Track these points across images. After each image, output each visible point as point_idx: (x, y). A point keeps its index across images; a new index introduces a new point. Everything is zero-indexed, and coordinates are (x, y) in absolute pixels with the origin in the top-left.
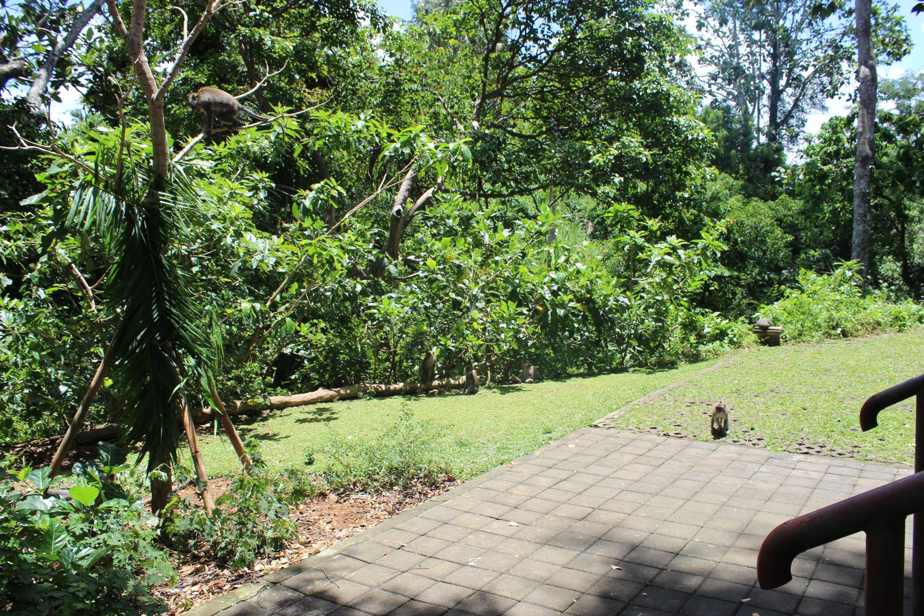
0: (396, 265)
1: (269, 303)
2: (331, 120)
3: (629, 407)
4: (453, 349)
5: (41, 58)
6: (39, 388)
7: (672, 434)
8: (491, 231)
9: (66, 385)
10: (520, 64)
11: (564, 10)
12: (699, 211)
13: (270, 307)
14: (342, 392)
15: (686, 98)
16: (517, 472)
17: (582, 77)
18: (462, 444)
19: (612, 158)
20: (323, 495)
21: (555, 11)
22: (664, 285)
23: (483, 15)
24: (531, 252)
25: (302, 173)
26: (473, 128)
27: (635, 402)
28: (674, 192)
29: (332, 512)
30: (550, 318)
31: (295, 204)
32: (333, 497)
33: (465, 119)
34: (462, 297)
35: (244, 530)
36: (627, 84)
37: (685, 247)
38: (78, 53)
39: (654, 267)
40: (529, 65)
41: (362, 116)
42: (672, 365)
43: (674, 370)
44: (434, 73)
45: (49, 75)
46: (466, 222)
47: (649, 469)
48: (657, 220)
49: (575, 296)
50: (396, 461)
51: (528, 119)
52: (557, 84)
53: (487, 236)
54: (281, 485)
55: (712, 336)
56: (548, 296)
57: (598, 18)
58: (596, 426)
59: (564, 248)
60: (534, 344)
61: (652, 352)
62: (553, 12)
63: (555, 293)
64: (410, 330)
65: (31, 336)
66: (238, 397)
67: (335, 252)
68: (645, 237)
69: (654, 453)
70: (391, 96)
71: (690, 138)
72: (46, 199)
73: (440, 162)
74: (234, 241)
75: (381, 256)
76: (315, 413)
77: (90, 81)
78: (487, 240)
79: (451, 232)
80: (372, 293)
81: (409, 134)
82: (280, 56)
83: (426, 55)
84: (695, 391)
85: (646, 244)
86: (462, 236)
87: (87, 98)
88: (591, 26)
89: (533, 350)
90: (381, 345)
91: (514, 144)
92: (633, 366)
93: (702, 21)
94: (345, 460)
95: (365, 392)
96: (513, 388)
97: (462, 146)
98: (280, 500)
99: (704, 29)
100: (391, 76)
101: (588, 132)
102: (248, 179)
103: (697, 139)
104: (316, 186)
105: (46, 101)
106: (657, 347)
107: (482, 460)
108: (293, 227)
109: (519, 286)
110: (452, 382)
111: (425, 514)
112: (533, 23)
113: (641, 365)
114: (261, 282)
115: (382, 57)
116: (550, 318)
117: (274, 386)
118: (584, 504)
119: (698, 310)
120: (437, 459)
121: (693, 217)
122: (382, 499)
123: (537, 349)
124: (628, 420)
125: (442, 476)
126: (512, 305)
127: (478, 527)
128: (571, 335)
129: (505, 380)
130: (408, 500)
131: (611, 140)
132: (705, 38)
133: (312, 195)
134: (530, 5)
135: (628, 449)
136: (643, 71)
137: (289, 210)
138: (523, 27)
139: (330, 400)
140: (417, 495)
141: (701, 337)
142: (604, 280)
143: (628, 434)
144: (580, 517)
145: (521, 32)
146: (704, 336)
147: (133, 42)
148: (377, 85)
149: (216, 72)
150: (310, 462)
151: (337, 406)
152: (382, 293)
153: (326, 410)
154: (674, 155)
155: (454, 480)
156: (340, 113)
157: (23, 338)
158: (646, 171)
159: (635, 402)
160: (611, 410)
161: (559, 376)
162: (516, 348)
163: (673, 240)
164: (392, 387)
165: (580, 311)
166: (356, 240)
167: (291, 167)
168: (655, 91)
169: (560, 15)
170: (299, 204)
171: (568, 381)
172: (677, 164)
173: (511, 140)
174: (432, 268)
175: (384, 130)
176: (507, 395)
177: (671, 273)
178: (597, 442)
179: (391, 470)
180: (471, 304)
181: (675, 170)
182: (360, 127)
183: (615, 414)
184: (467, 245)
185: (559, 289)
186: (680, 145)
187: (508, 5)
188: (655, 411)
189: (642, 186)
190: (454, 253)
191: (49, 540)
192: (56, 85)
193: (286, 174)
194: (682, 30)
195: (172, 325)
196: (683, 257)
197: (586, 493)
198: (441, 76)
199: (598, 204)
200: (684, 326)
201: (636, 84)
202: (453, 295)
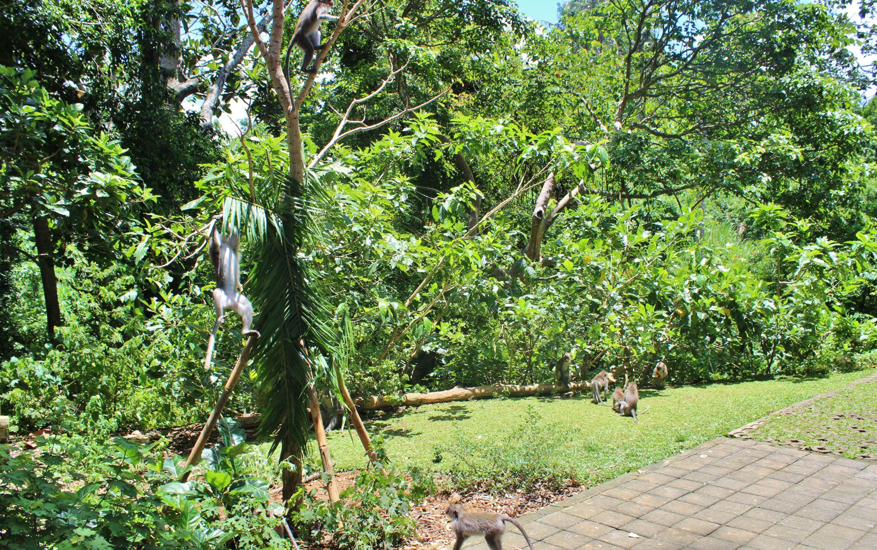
0: (534, 267)
1: (408, 303)
2: (470, 125)
3: (769, 418)
4: (590, 352)
5: (215, 74)
6: (193, 378)
7: (815, 448)
8: (630, 233)
9: (216, 375)
10: (665, 62)
11: (709, 7)
12: (857, 209)
13: (409, 306)
14: (477, 391)
15: (841, 90)
17: (728, 73)
18: (590, 449)
19: (759, 156)
21: (699, 8)
22: (814, 289)
23: (625, 16)
24: (672, 255)
25: (449, 175)
26: (616, 128)
27: (776, 413)
28: (828, 190)
30: (690, 322)
31: (435, 207)
33: (608, 119)
34: (600, 299)
36: (777, 79)
37: (836, 249)
38: (246, 68)
39: (802, 270)
40: (673, 64)
42: (822, 374)
43: (824, 379)
44: (577, 75)
45: (220, 89)
46: (607, 223)
47: (786, 485)
48: (807, 220)
49: (717, 299)
50: (520, 463)
51: (672, 118)
52: (701, 82)
53: (625, 238)
54: (403, 482)
55: (870, 343)
56: (688, 299)
57: (745, 12)
58: (732, 436)
59: (716, 251)
60: (674, 348)
61: (802, 358)
62: (697, 9)
63: (695, 297)
64: (546, 332)
65: (188, 329)
66: (375, 392)
67: (470, 253)
68: (793, 239)
69: (794, 468)
70: (534, 99)
71: (846, 133)
72: (203, 204)
73: (577, 163)
74: (373, 243)
75: (520, 257)
76: (448, 411)
77: (256, 93)
78: (625, 241)
79: (590, 235)
80: (510, 294)
81: (547, 136)
82: (424, 64)
83: (568, 57)
84: (845, 404)
85: (794, 247)
86: (602, 237)
87: (252, 109)
88: (737, 21)
89: (674, 354)
90: (518, 346)
91: (657, 143)
92: (780, 373)
93: (866, 7)
94: (471, 460)
95: (500, 392)
96: (650, 393)
97: (599, 147)
98: (400, 497)
99: (868, 16)
100: (535, 79)
101: (734, 130)
102: (390, 183)
103: (854, 134)
104: (455, 189)
105: (216, 112)
106: (807, 354)
107: (609, 466)
108: (432, 227)
109: (658, 288)
110: (588, 384)
111: (544, 519)
112: (676, 20)
113: (788, 373)
114: (401, 282)
115: (527, 62)
116: (690, 322)
117: (412, 382)
118: (710, 519)
119: (857, 315)
120: (563, 462)
121: (850, 217)
123: (678, 353)
124: (767, 431)
125: (567, 481)
126: (651, 308)
127: (596, 536)
128: (713, 340)
130: (530, 503)
131: (758, 138)
132: (870, 25)
133: (451, 197)
134: (673, 4)
135: (764, 462)
136: (793, 65)
138: (666, 25)
139: (465, 399)
140: (540, 499)
141: (856, 346)
142: (748, 283)
143: (766, 446)
144: (705, 533)
145: (664, 31)
146: (861, 344)
147: (271, 58)
148: (521, 88)
149: (366, 80)
150: (438, 460)
151: (471, 405)
152: (519, 294)
153: (459, 408)
154: (827, 152)
155: (579, 485)
156: (480, 118)
157: (181, 331)
158: (798, 169)
159: (776, 413)
160: (750, 420)
161: (698, 381)
162: (654, 352)
163: (823, 241)
164: (527, 388)
165: (721, 315)
166: (494, 242)
167: (438, 170)
168: (806, 85)
169: (704, 11)
170: (438, 207)
171: (709, 387)
172: (831, 160)
173: (654, 139)
174: (569, 270)
175: (524, 133)
177: (821, 276)
178: (731, 454)
179: (514, 473)
180: (609, 306)
181: (829, 167)
182: (498, 132)
183: (754, 425)
184: (606, 247)
185: (700, 292)
186: (835, 141)
187: (650, 4)
188: (798, 423)
189: (793, 185)
190: (593, 256)
191: (184, 519)
192: (227, 98)
193: (429, 177)
194: (842, 20)
195: (305, 324)
196: (835, 259)
197: (714, 508)
198: (584, 78)
199: (747, 204)
200: (838, 332)
201: (786, 79)
202: (590, 297)
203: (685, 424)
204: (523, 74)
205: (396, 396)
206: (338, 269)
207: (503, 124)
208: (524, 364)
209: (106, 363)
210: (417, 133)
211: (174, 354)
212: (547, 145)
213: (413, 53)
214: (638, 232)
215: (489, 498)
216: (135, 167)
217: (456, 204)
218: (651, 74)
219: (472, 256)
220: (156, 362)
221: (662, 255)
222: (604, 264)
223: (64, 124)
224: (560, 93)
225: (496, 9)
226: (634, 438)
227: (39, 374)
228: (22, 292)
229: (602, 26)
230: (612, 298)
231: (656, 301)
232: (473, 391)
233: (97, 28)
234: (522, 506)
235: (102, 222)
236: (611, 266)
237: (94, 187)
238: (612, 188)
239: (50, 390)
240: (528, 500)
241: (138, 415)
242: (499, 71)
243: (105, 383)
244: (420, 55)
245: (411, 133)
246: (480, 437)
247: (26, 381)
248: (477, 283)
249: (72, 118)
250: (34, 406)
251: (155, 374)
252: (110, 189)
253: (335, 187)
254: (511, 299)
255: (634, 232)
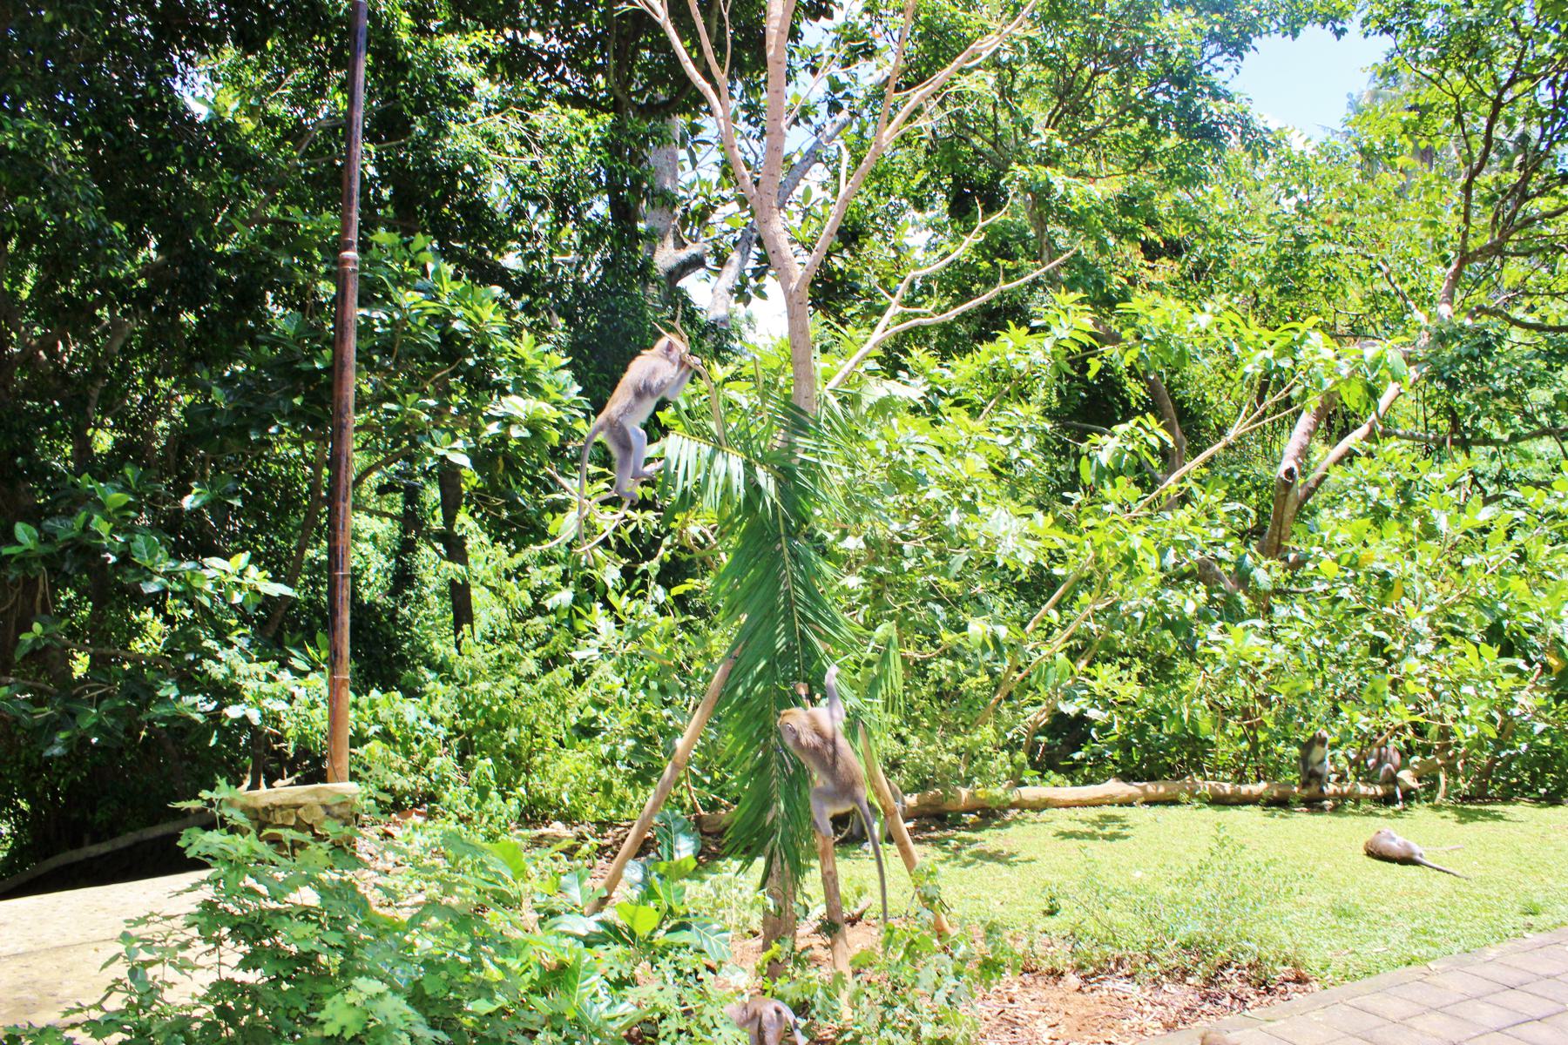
0: (1268, 570)
8: (1454, 510)
16: (1435, 986)
18: (1343, 913)
20: (1057, 975)
25: (1134, 403)
29: (1063, 1008)
31: (1084, 459)
32: (1073, 980)
34: (1388, 631)
35: (889, 1017)
41: (1208, 306)
50: (1194, 928)
66: (967, 782)
76: (1093, 823)
78: (1442, 524)
79: (1379, 514)
80: (1220, 618)
82: (1080, 209)
83: (1353, 189)
89: (1547, 742)
96: (1486, 814)
98: (957, 974)
100: (1289, 231)
104: (1119, 429)
109: (1507, 615)
122: (1160, 997)
125: (1284, 971)
126: (1491, 652)
129: (1478, 795)
130: (1207, 1006)
137: (1073, 469)
140: (1227, 1001)
145: (1543, 131)
148: (1263, 249)
150: (1051, 912)
155: (1307, 981)
164: (1245, 789)
170: (1090, 459)
173: (1517, 334)
176: (1469, 825)
182: (1203, 327)
190: (1382, 553)
191: (571, 978)
203: (1549, 881)
204: (1269, 222)
205: (998, 791)
206: (906, 565)
207: (1213, 313)
208: (1245, 745)
209: (515, 707)
210: (1055, 329)
211: (620, 700)
212: (1291, 350)
213: (1061, 190)
214: (1468, 509)
215: (1133, 989)
216: (580, 389)
217: (1122, 454)
218: (1514, 214)
219: (1142, 548)
220: (591, 712)
221: (1518, 552)
222: (1401, 568)
223: (470, 322)
224: (1337, 254)
225: (1211, 108)
226: (1436, 898)
227: (410, 718)
228: (432, 587)
229: (1416, 131)
230: (1414, 631)
231: (1503, 639)
232: (1144, 789)
233: (534, 166)
234: (1191, 1010)
235: (528, 476)
236: (1415, 571)
237: (507, 421)
238: (1436, 426)
239: (427, 746)
240: (1204, 999)
241: (564, 796)
242: (1223, 218)
243: (512, 741)
244: (1073, 193)
245: (1046, 329)
246: (1138, 874)
247: (393, 729)
248: (1156, 596)
249: (479, 309)
250: (401, 771)
251: (586, 731)
252: (534, 426)
253: (894, 421)
254: (1224, 627)
255: (1462, 509)
